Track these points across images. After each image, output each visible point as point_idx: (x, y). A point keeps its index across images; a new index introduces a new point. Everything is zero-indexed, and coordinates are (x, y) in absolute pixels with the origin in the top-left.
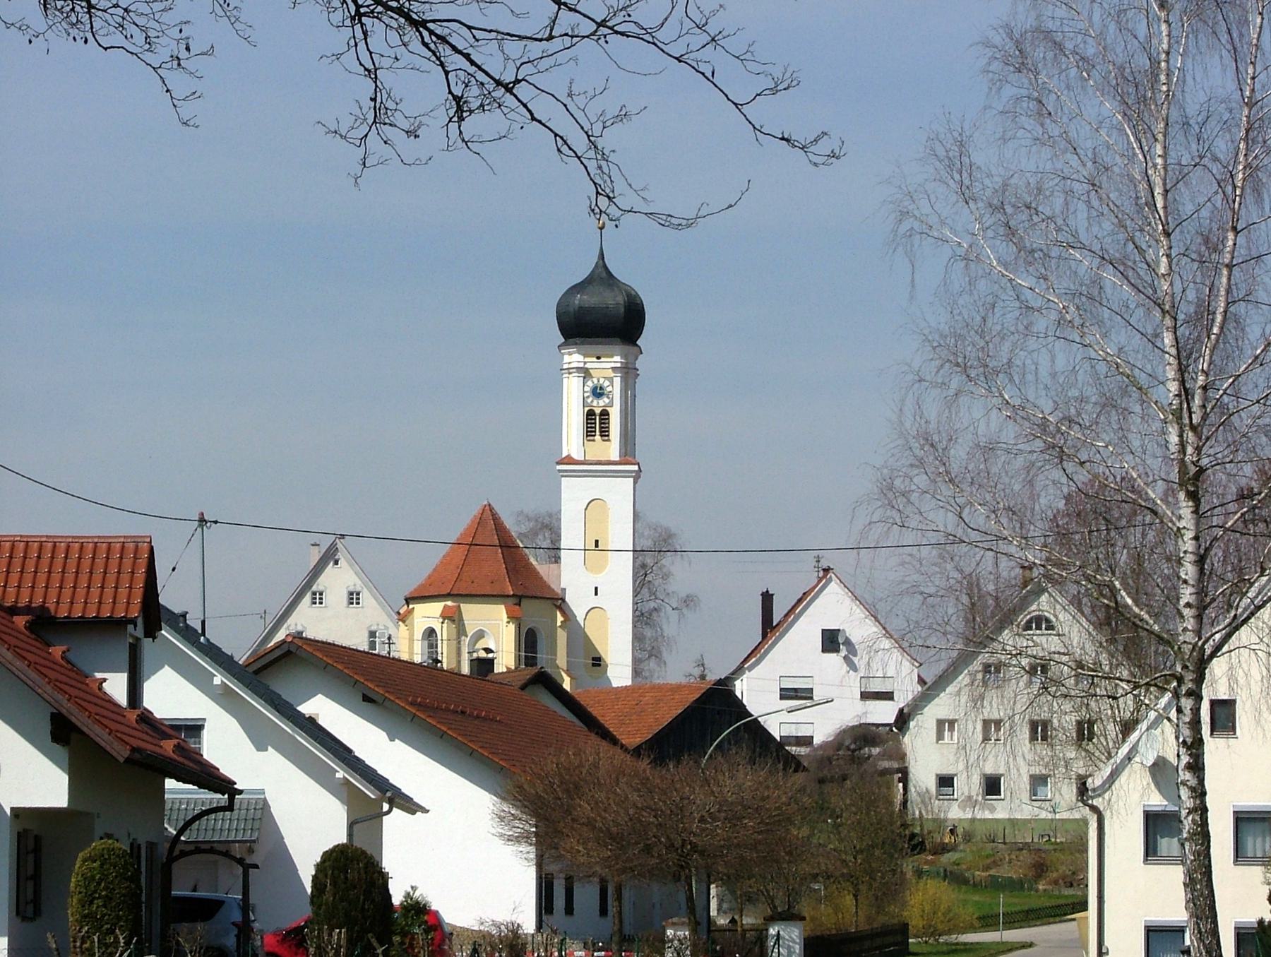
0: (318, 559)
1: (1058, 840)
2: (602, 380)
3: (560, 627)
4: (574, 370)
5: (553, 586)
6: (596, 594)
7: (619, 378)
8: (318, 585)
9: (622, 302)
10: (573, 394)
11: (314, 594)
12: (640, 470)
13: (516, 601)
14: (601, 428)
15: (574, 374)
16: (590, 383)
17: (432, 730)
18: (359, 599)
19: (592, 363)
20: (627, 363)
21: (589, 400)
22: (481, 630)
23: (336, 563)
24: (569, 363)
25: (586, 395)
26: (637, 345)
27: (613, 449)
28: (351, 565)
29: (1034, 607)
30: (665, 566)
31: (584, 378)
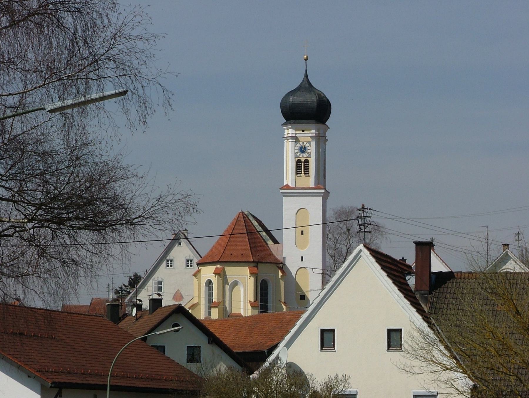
1: (269, 388)
2: (305, 143)
4: (290, 138)
6: (302, 260)
7: (314, 142)
8: (170, 256)
9: (316, 100)
10: (289, 148)
11: (168, 261)
13: (255, 264)
14: (305, 169)
15: (290, 140)
16: (298, 145)
18: (192, 263)
19: (299, 134)
20: (319, 134)
21: (298, 154)
23: (180, 244)
24: (287, 134)
25: (296, 151)
27: (311, 181)
29: (504, 268)
30: (377, 244)
31: (295, 142)
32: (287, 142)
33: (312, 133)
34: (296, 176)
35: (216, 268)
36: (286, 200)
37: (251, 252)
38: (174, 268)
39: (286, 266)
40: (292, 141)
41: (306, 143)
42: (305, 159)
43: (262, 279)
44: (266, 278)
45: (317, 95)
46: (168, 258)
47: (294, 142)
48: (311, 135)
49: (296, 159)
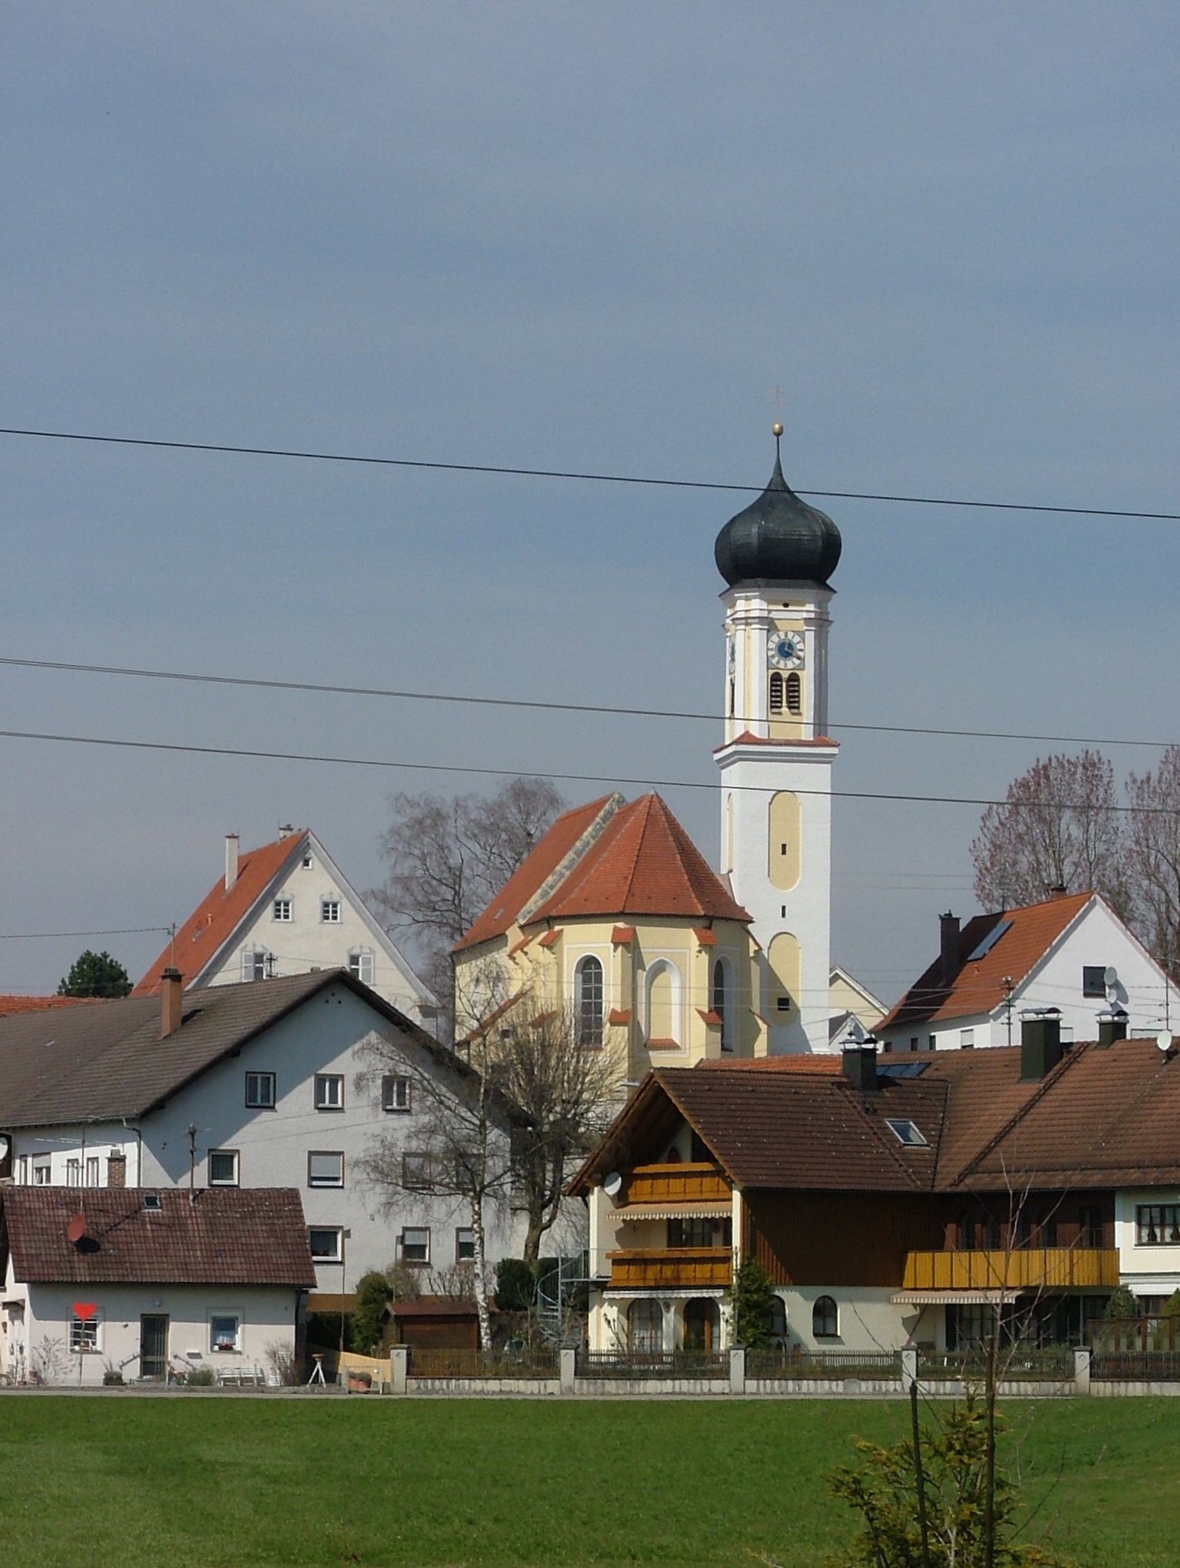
2: (790, 635)
3: (753, 958)
4: (757, 620)
7: (813, 633)
11: (278, 904)
13: (705, 923)
14: (788, 697)
15: (754, 626)
16: (775, 638)
19: (778, 613)
21: (774, 661)
22: (662, 960)
23: (306, 863)
24: (746, 611)
25: (770, 653)
31: (768, 631)
41: (792, 634)
46: (278, 897)
47: (765, 632)
48: (805, 615)
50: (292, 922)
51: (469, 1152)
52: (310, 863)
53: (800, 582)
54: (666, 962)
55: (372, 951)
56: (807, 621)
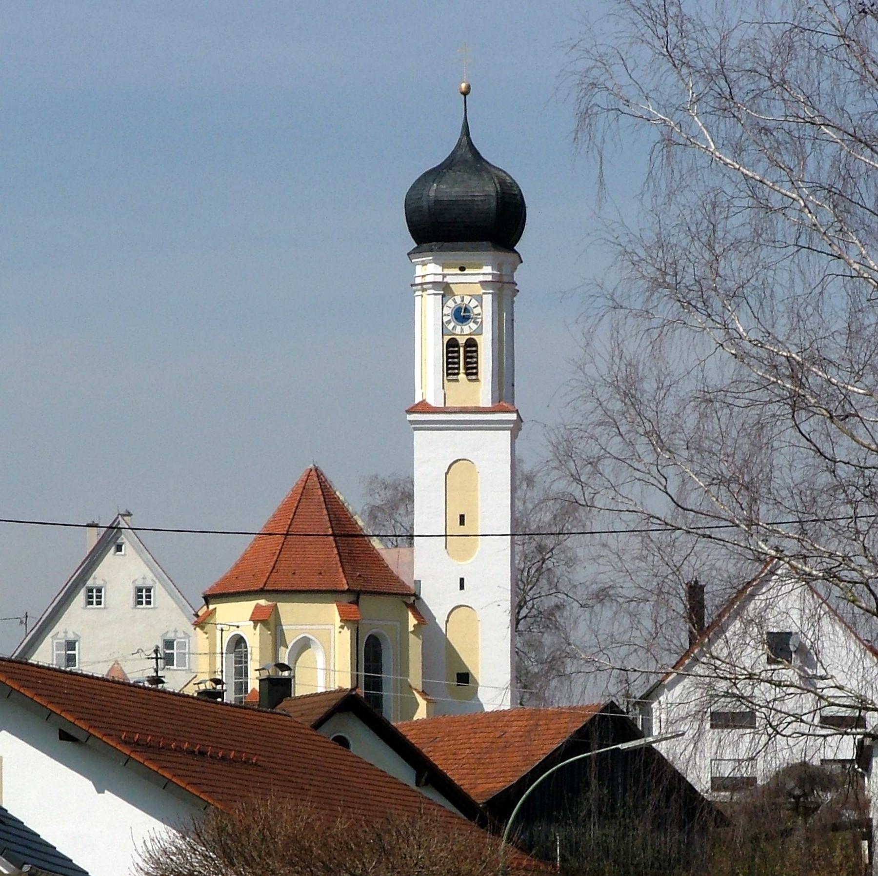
0: (96, 542)
2: (467, 299)
3: (412, 632)
4: (430, 286)
5: (403, 578)
6: (462, 587)
7: (490, 296)
8: (95, 578)
9: (494, 194)
11: (90, 590)
12: (520, 419)
13: (352, 598)
14: (466, 363)
16: (451, 303)
17: (150, 776)
19: (453, 277)
20: (501, 275)
21: (450, 327)
23: (119, 548)
24: (423, 276)
25: (446, 319)
26: (516, 252)
28: (139, 553)
31: (443, 296)
32: (422, 296)
33: (484, 274)
34: (446, 381)
35: (256, 607)
36: (420, 437)
37: (342, 566)
38: (105, 608)
39: (423, 602)
40: (435, 294)
41: (469, 298)
42: (450, 337)
43: (369, 634)
44: (374, 630)
45: (496, 181)
47: (441, 296)
48: (482, 278)
49: (445, 337)
50: (105, 608)
51: (735, 794)
52: (123, 547)
53: (475, 244)
54: (309, 639)
55: (187, 636)
56: (483, 283)
